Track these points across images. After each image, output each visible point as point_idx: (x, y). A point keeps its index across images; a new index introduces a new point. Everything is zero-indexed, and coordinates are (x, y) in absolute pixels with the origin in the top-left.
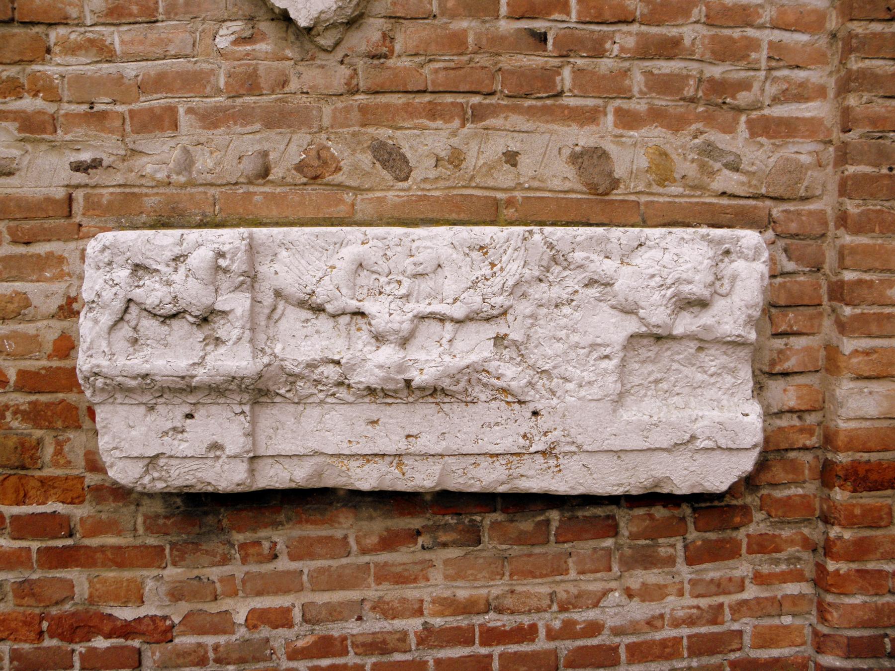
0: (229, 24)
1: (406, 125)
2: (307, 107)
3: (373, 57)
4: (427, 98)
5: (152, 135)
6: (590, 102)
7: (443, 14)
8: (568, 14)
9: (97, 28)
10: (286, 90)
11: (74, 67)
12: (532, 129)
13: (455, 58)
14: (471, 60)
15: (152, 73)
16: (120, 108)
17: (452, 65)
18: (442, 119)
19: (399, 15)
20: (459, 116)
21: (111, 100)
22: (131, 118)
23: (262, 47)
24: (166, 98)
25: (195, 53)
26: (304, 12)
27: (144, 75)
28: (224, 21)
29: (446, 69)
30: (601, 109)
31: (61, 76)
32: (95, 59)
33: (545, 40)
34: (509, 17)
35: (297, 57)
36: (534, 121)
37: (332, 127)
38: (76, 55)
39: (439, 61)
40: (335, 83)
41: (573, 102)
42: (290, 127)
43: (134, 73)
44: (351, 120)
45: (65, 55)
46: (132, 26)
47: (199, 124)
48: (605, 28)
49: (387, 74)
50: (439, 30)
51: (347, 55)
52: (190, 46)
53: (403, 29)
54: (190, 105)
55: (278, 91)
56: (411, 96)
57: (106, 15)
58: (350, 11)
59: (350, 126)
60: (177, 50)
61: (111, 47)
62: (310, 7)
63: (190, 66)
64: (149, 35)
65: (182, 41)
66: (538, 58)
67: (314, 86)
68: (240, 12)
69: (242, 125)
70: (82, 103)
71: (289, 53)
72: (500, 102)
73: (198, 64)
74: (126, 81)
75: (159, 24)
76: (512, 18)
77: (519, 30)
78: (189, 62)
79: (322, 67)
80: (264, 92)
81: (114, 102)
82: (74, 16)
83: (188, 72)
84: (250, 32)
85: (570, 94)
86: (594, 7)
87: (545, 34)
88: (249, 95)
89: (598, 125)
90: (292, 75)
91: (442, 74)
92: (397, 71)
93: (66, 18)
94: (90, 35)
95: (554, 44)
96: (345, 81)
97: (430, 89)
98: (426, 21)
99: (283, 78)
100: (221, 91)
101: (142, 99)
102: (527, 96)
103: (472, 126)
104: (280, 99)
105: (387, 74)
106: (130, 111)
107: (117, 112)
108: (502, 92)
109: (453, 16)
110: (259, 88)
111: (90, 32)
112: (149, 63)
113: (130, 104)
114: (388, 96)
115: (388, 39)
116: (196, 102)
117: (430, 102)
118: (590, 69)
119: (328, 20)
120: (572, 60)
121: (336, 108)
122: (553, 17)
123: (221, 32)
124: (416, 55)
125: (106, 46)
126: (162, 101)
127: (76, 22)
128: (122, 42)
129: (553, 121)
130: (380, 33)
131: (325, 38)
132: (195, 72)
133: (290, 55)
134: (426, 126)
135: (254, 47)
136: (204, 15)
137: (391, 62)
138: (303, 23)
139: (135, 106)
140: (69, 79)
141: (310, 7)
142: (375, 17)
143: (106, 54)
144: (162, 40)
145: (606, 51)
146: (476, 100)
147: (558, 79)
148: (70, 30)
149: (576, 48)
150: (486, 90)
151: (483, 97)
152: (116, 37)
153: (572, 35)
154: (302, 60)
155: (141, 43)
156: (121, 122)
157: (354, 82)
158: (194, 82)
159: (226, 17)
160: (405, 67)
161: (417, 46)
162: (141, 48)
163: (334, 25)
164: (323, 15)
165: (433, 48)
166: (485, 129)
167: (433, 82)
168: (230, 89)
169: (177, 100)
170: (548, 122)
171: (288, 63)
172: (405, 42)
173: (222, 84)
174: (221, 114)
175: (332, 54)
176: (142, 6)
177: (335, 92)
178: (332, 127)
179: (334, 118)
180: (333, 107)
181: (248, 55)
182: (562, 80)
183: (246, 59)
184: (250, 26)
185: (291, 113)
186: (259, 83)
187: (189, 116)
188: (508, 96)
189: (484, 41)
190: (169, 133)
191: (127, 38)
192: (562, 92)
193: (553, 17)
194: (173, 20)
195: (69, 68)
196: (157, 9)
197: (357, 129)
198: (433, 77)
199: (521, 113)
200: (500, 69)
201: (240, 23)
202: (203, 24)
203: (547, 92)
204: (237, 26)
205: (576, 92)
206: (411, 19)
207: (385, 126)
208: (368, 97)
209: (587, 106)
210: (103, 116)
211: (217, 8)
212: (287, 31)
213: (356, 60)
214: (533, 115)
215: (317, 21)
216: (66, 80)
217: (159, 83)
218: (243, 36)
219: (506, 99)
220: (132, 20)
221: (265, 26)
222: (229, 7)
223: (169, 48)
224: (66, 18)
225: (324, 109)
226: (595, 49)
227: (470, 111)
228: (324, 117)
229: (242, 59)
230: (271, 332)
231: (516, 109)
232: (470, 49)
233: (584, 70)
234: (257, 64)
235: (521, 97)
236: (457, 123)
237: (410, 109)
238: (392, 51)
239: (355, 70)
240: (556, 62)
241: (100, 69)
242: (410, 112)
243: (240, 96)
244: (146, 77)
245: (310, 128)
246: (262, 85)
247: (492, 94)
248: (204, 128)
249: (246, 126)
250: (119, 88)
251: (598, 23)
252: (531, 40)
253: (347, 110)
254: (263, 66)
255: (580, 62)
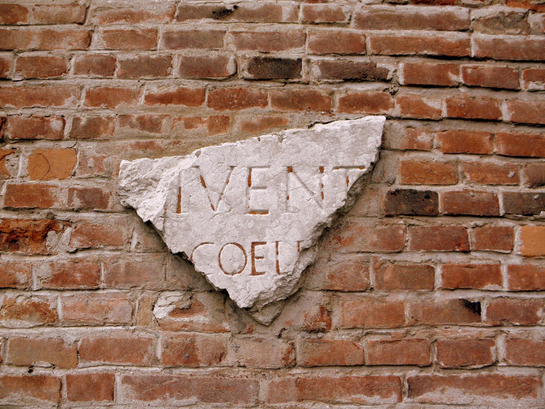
0: (167, 294)
1: (343, 400)
2: (244, 382)
3: (311, 332)
4: (364, 372)
5: (89, 403)
6: (525, 372)
7: (380, 287)
8: (500, 283)
9: (43, 293)
10: (224, 362)
11: (17, 330)
12: (469, 402)
13: (392, 331)
14: (408, 332)
15: (91, 339)
16: (59, 373)
17: (389, 338)
18: (379, 394)
19: (336, 288)
20: (395, 391)
21: (50, 365)
22: (69, 385)
23: (199, 318)
24: (103, 365)
25: (134, 321)
26: (243, 293)
27: (83, 341)
28: (163, 291)
29: (383, 342)
30: (537, 379)
31: (4, 338)
32: (39, 324)
33: (479, 311)
34: (445, 289)
35: (235, 329)
36: (471, 394)
37: (269, 401)
38: (20, 319)
39: (376, 334)
40: (273, 358)
41: (508, 372)
42: (226, 401)
43: (74, 339)
44: (288, 395)
45: (11, 318)
46: (74, 293)
47: (135, 394)
48: (535, 296)
49: (324, 348)
50: (376, 303)
51: (284, 329)
52: (129, 315)
53: (340, 302)
54: (126, 374)
55: (215, 364)
56: (349, 370)
57: (52, 281)
58: (290, 290)
59: (286, 401)
60: (116, 319)
61: (54, 312)
62: (250, 288)
63: (128, 335)
64: (90, 302)
65: (121, 309)
66: (473, 329)
67: (251, 359)
68: (179, 283)
69: (178, 398)
70: (22, 366)
71: (226, 325)
72: (437, 374)
73: (137, 332)
74: (66, 346)
75: (100, 292)
76: (447, 289)
77: (453, 301)
78: (127, 330)
79: (260, 341)
80: (201, 365)
81: (53, 366)
82: (22, 281)
83: (126, 340)
84: (188, 303)
85: (505, 364)
86: (525, 276)
87: (479, 304)
88: (185, 367)
89: (535, 396)
90: (229, 348)
91: (379, 348)
92: (334, 345)
93: (15, 283)
94: (35, 300)
95: (488, 314)
96: (283, 356)
97: (368, 362)
98: (363, 294)
99: (220, 351)
100: (158, 360)
101: (80, 365)
102: (462, 368)
103: (409, 400)
104: (216, 372)
105: (324, 348)
106: (68, 377)
107: (55, 378)
108: (437, 364)
109: (390, 289)
110: (196, 361)
111: (35, 296)
112: (89, 329)
113: (68, 369)
114: (325, 369)
115: (326, 313)
116: (133, 371)
117: (367, 377)
118: (523, 338)
119: (267, 299)
120: (505, 329)
121: (273, 382)
122: (486, 287)
123: (161, 302)
124: (354, 328)
125: (49, 311)
126: (100, 368)
127: (23, 287)
128: (65, 308)
129: (489, 393)
130: (318, 307)
131: (263, 315)
132: (133, 340)
133: (227, 328)
134: (363, 401)
135: (192, 319)
136: (143, 285)
137: (328, 336)
138: (242, 304)
139: (72, 372)
140: (11, 342)
141: (250, 288)
142: (313, 290)
143: (48, 317)
144: (102, 308)
145: (538, 319)
146: (413, 373)
147: (492, 349)
148: (18, 294)
149: (508, 317)
150: (422, 363)
151: (419, 369)
152: (58, 302)
153: (505, 304)
154: (239, 333)
155: (83, 309)
156: (58, 388)
157: (292, 356)
158: (132, 351)
159: (164, 287)
160: (342, 341)
161: (355, 320)
162: (82, 314)
163: (273, 304)
164: (263, 296)
165: (370, 321)
166: (422, 403)
167: (370, 356)
168: (167, 360)
169: (114, 368)
170: (484, 394)
171: (225, 335)
172: (343, 316)
173: (159, 355)
174: (157, 385)
175: (270, 328)
176: (86, 274)
177: (273, 366)
178: (269, 401)
179: (271, 392)
180: (270, 381)
181: (185, 326)
182: (496, 350)
183: (184, 331)
184: (188, 297)
185: (227, 387)
186: (196, 356)
187: (126, 385)
188: (444, 368)
189: (421, 314)
190: (105, 402)
191: (69, 303)
192: (497, 361)
193: (486, 287)
194: (114, 288)
195: (13, 331)
196: (99, 277)
197: (294, 403)
198: (370, 350)
199: (457, 386)
200: (436, 341)
201: (178, 294)
202: (142, 293)
203: (482, 363)
204: (175, 297)
205: (510, 362)
206: (349, 292)
207: (322, 401)
208: (306, 371)
209: (522, 376)
210: (41, 380)
211: (157, 278)
212: (224, 303)
213: (293, 334)
214: (469, 388)
215: (257, 301)
216: (8, 342)
217: (96, 350)
218: (181, 307)
219: (441, 371)
220: (75, 287)
221: (202, 297)
222: (168, 278)
223: (109, 316)
224: (15, 283)
225: (260, 383)
226: (527, 318)
227: (406, 385)
228: (261, 391)
229: (180, 330)
230: (170, 115)
231: (452, 382)
232: (407, 322)
233: (517, 339)
234: (194, 336)
235: (457, 369)
236: (394, 397)
237: (347, 384)
238: (329, 325)
239: (293, 344)
240: (489, 332)
241: (42, 334)
242: (347, 386)
243: (176, 367)
244: (86, 343)
245: (247, 402)
246: (199, 358)
247: (430, 366)
248: (141, 399)
249: (182, 398)
250: (59, 353)
251: (529, 291)
252: (466, 311)
253: (285, 384)
254: (201, 337)
255: (513, 331)
